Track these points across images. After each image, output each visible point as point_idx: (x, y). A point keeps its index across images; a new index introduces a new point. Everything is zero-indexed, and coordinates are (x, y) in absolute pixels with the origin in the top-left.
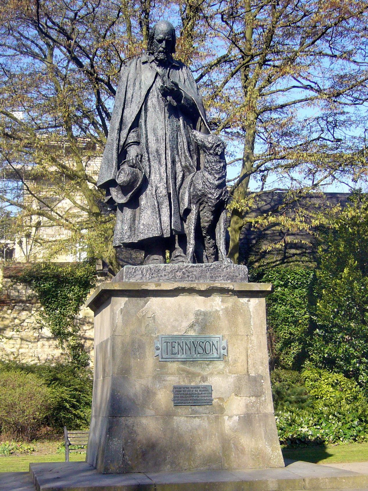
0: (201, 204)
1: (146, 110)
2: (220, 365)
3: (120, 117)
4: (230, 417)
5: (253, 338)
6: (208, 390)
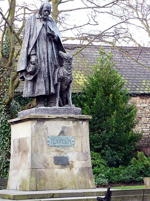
0: (62, 81)
1: (39, 40)
2: (72, 148)
3: (28, 43)
4: (76, 169)
5: (84, 137)
6: (67, 158)
